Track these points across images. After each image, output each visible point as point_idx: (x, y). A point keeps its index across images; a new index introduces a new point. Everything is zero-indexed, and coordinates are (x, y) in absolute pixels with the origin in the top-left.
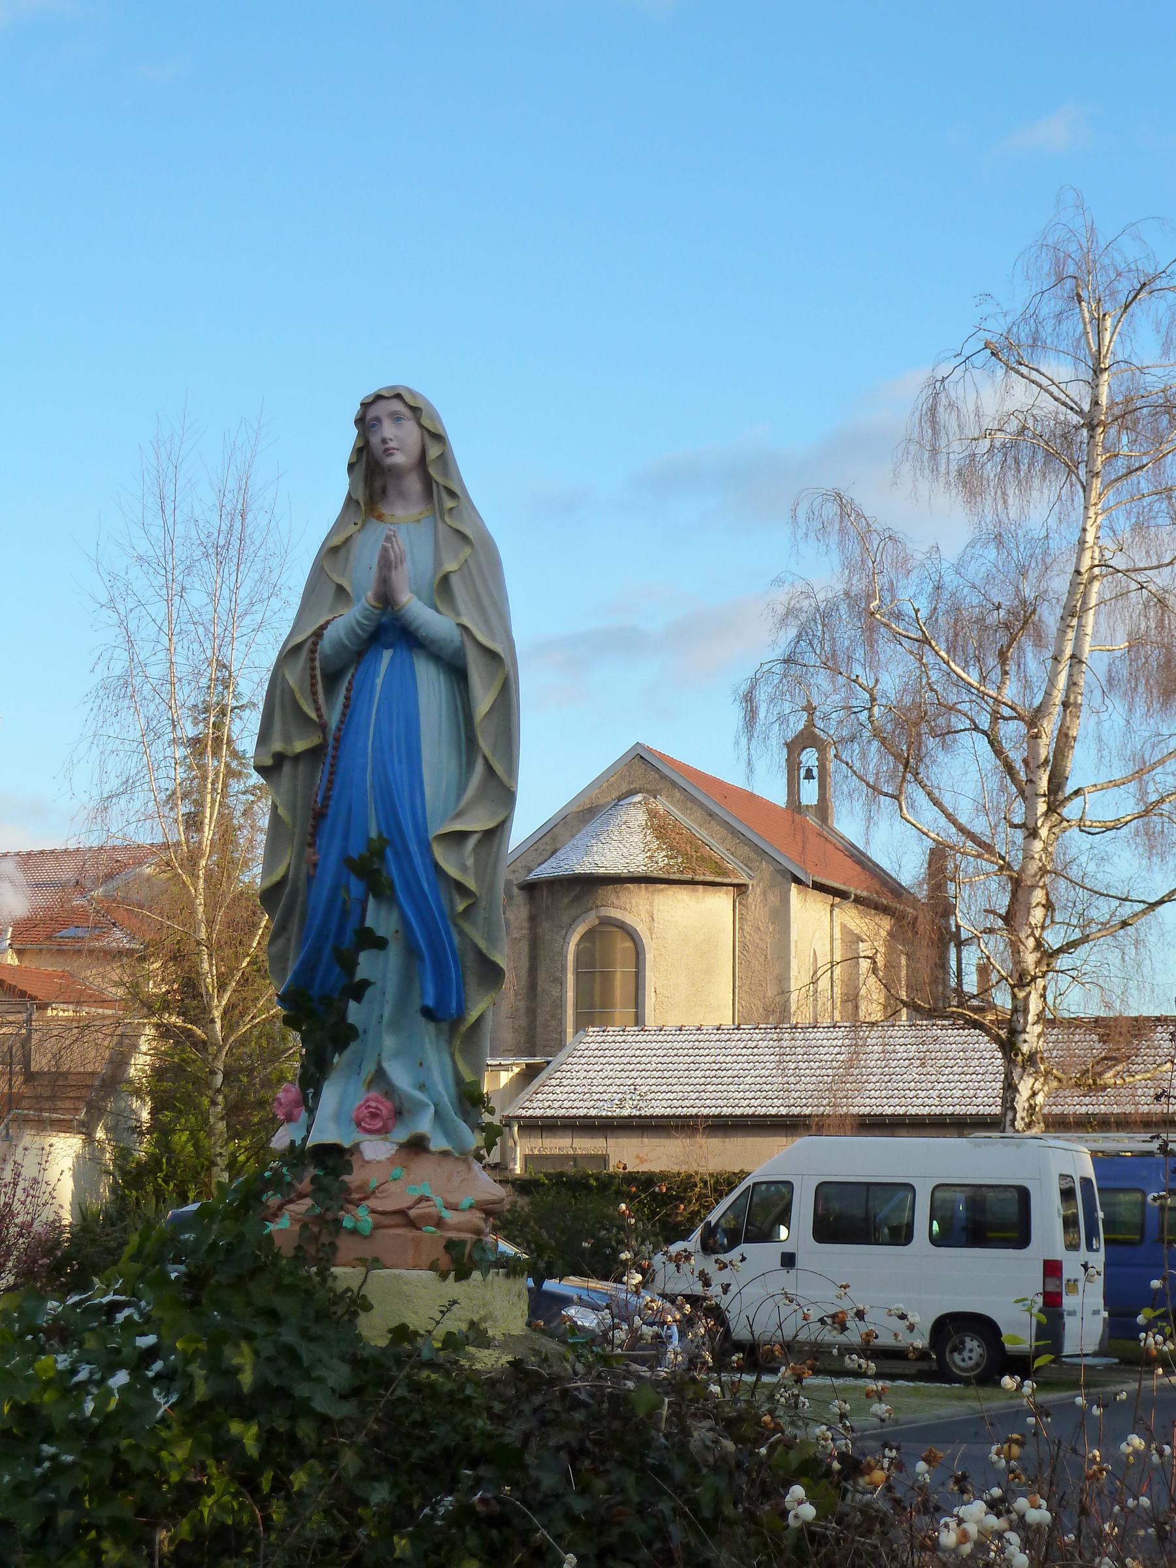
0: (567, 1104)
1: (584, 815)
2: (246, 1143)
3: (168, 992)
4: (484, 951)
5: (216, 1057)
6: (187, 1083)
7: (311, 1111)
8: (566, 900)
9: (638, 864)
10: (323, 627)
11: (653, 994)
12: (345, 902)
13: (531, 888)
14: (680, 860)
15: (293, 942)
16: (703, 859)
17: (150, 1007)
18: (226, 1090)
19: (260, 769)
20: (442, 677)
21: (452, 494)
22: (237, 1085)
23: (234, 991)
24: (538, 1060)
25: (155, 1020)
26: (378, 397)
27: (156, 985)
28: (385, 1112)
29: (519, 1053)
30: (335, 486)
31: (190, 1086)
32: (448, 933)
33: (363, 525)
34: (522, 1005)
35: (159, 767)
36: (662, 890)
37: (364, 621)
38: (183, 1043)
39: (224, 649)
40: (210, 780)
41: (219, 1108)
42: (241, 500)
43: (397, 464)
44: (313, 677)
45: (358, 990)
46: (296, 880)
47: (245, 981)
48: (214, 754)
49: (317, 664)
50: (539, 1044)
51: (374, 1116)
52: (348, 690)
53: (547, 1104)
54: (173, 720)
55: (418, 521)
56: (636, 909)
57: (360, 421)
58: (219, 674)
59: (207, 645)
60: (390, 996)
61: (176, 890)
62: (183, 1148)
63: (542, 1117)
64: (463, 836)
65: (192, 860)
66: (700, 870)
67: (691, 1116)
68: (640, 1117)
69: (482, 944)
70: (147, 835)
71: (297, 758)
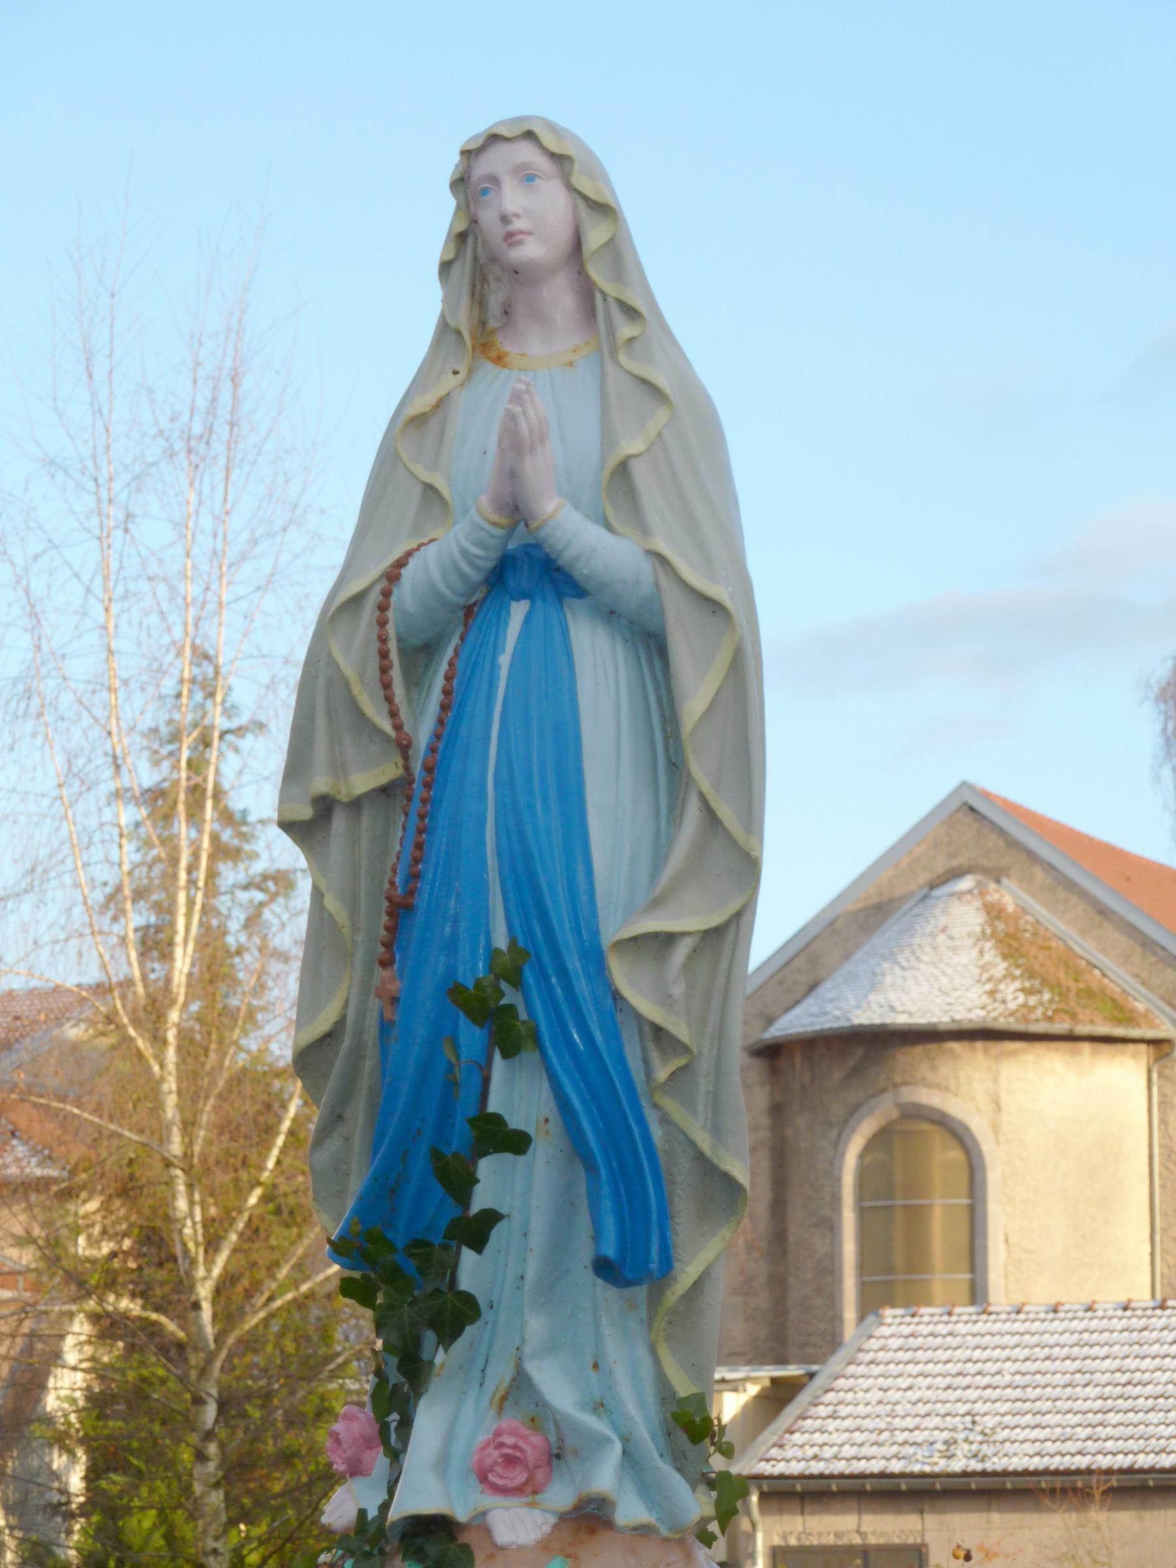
0: (848, 1451)
1: (868, 917)
2: (262, 1529)
3: (113, 1255)
4: (708, 1152)
5: (203, 1372)
6: (152, 1421)
7: (396, 1456)
8: (837, 1075)
9: (967, 1005)
10: (401, 563)
11: (1002, 1246)
12: (450, 1067)
13: (771, 1053)
14: (1047, 996)
15: (357, 1143)
16: (1089, 994)
17: (81, 1282)
18: (223, 1433)
19: (288, 826)
20: (620, 650)
21: (632, 313)
22: (242, 1424)
23: (235, 1251)
24: (792, 1371)
25: (91, 1304)
26: (493, 139)
27: (93, 1242)
28: (531, 1455)
29: (756, 1358)
30: (417, 304)
31: (157, 1428)
32: (642, 1123)
33: (471, 372)
34: (761, 1270)
35: (90, 843)
36: (1015, 1053)
37: (475, 550)
38: (141, 1349)
39: (205, 625)
40: (183, 864)
41: (211, 1466)
42: (230, 352)
43: (527, 263)
44: (384, 655)
45: (478, 1230)
46: (360, 1030)
47: (253, 1232)
48: (190, 817)
49: (391, 629)
50: (794, 1338)
51: (510, 1461)
52: (448, 678)
53: (810, 1452)
54: (115, 757)
55: (571, 364)
56: (966, 1088)
57: (460, 183)
58: (196, 671)
59: (174, 618)
60: (537, 1241)
61: (124, 1067)
62: (147, 1540)
63: (802, 1477)
64: (668, 939)
65: (152, 1013)
66: (1084, 1015)
67: (1078, 1472)
68: (984, 1474)
69: (704, 1141)
70: (74, 970)
71: (356, 804)
